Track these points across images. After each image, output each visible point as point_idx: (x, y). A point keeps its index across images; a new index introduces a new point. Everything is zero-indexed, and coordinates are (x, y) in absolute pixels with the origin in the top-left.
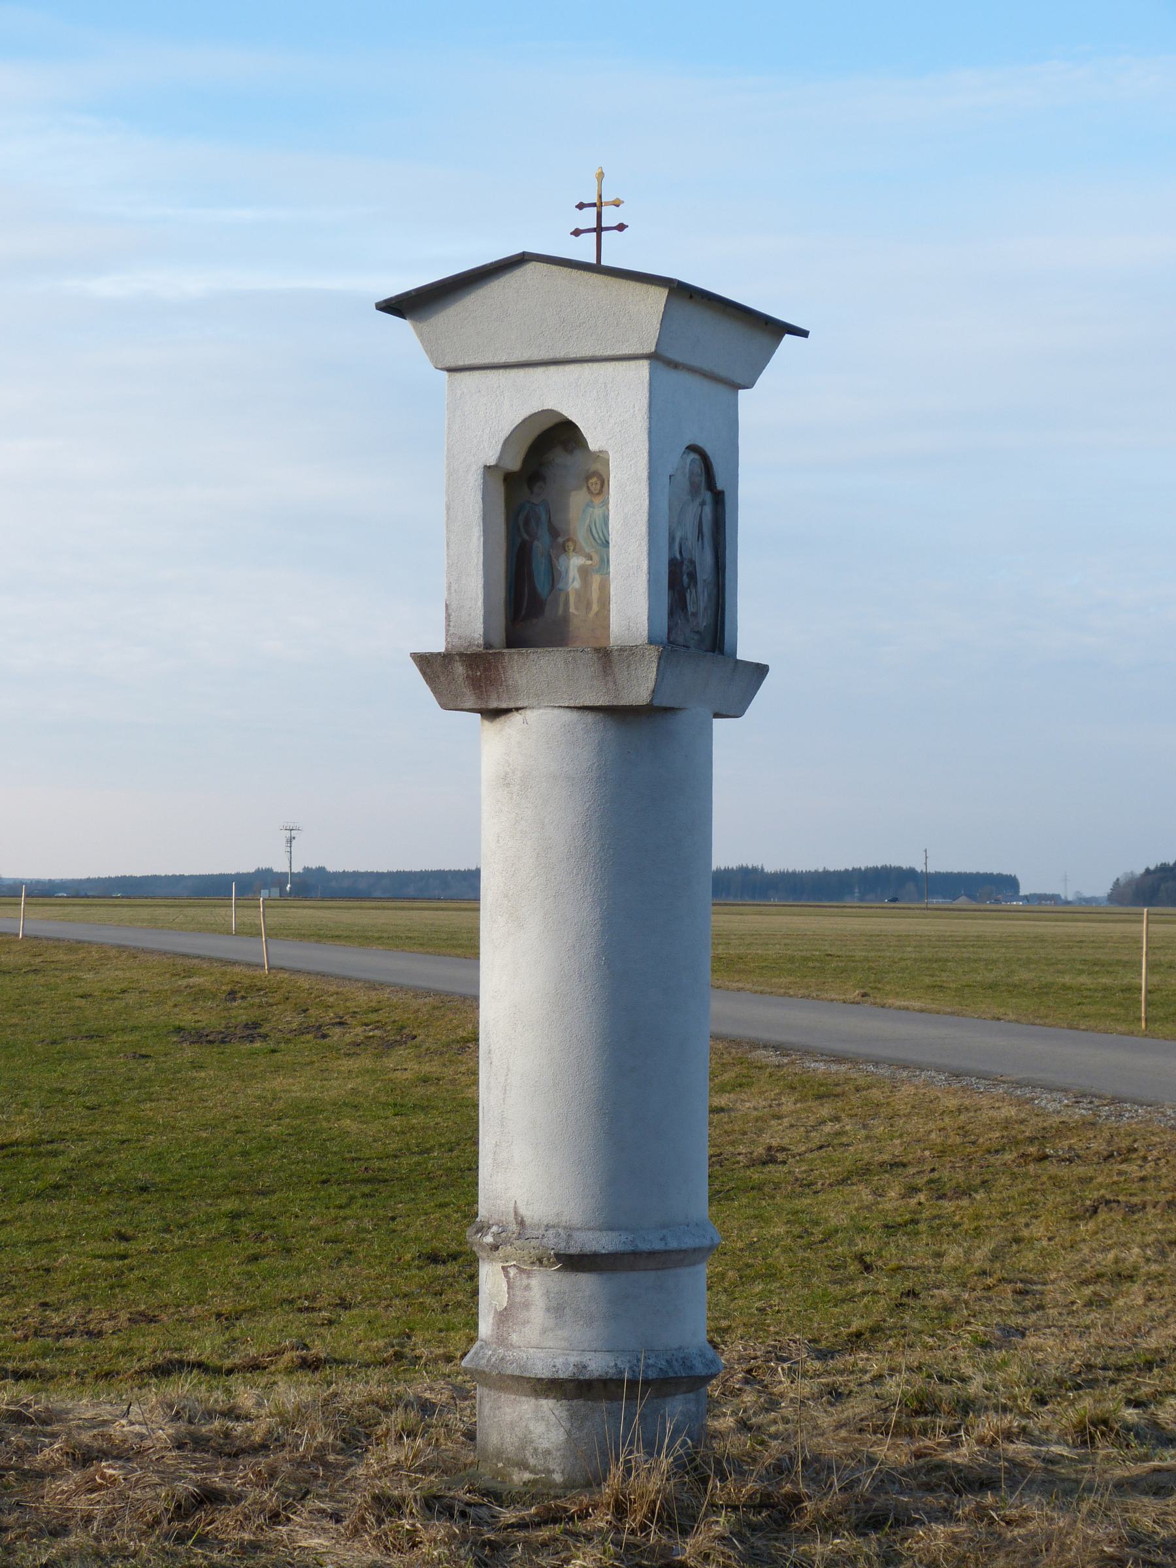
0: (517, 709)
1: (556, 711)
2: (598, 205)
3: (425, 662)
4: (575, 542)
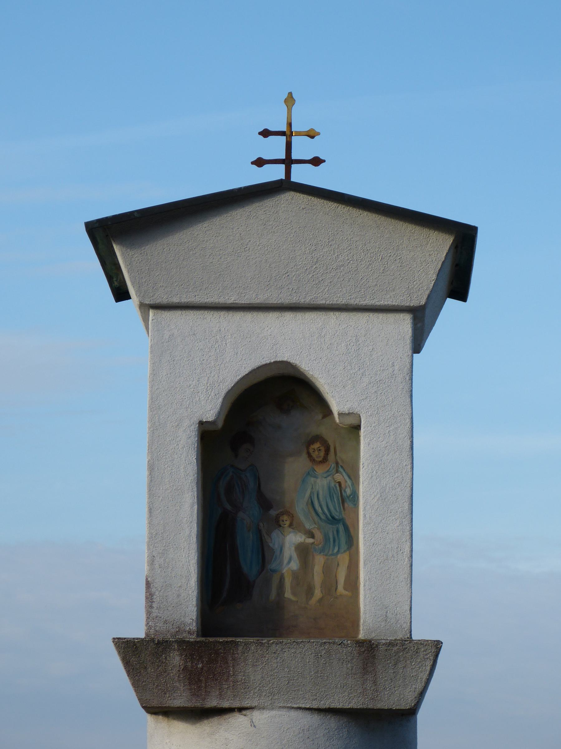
0: (241, 710)
1: (294, 714)
2: (288, 134)
3: (128, 649)
4: (292, 516)
